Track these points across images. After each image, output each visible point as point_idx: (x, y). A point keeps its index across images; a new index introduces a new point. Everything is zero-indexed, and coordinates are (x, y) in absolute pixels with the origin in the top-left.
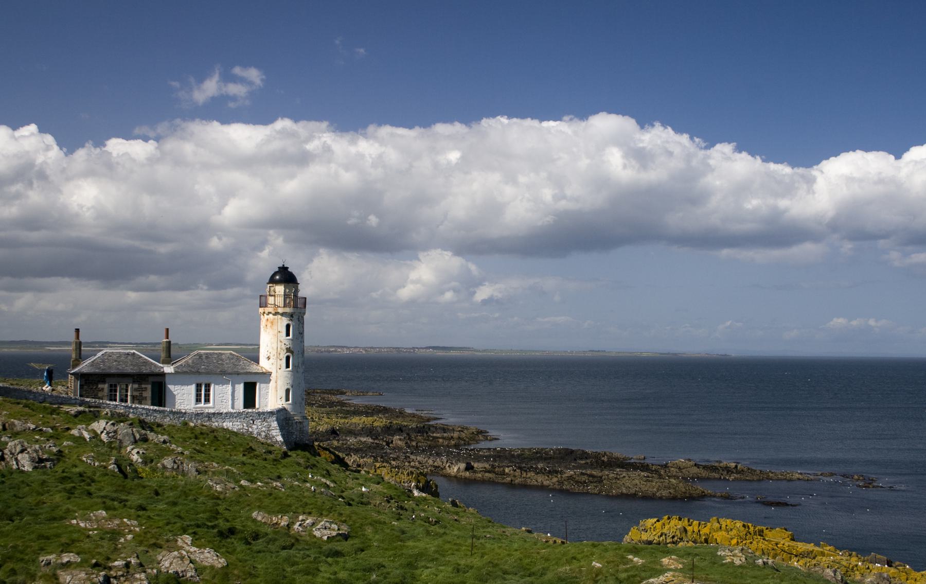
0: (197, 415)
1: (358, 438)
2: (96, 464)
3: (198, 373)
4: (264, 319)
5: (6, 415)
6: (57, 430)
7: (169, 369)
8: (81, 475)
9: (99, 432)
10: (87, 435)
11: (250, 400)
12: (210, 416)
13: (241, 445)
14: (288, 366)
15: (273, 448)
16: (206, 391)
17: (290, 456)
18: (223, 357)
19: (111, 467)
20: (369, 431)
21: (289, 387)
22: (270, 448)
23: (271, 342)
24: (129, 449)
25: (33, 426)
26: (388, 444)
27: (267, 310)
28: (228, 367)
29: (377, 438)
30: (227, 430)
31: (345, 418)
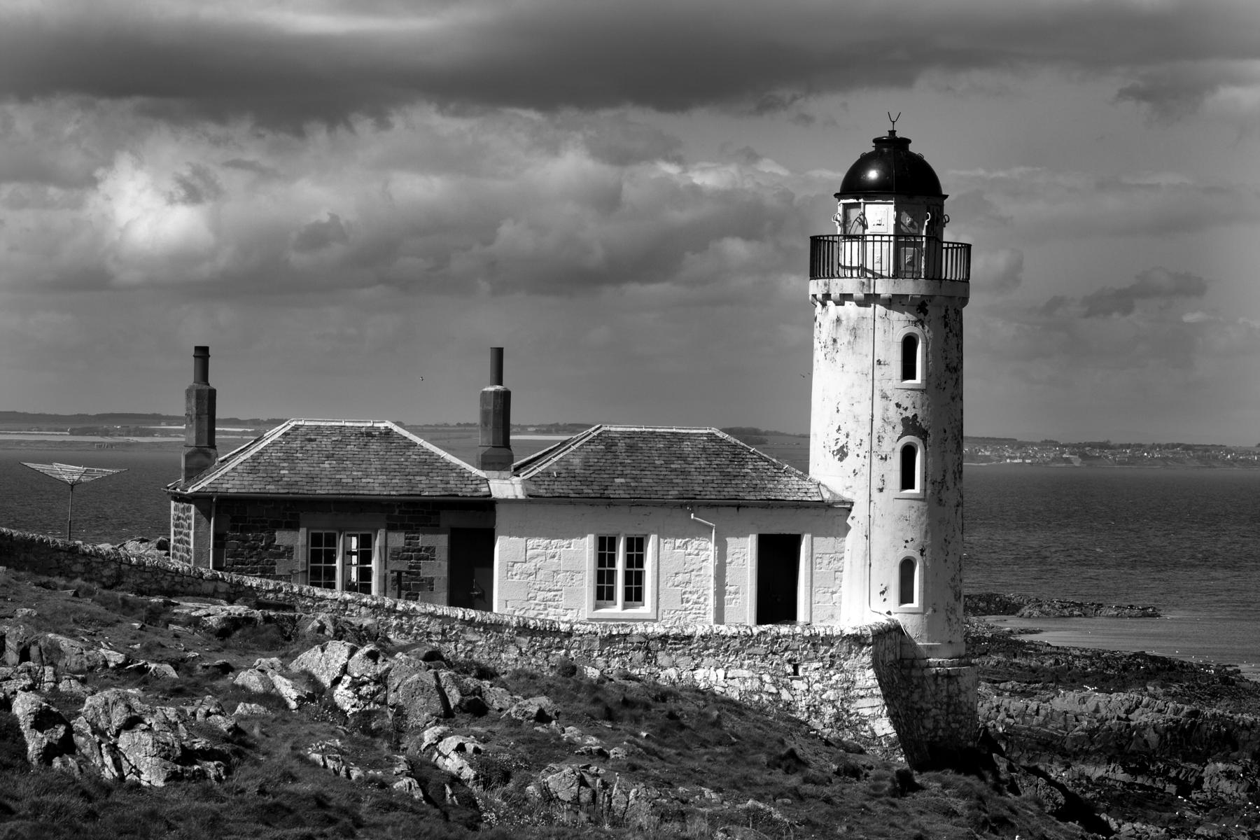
0: (609, 639)
1: (1078, 767)
2: (356, 773)
3: (604, 501)
4: (826, 316)
5: (27, 619)
6: (190, 671)
7: (505, 487)
8: (320, 801)
9: (326, 681)
10: (289, 691)
11: (776, 598)
12: (650, 646)
13: (759, 745)
14: (907, 482)
15: (862, 761)
16: (629, 562)
17: (919, 788)
18: (687, 447)
19: (402, 784)
20: (1118, 744)
21: (912, 552)
22: (853, 759)
23: (847, 393)
24: (428, 736)
25: (116, 658)
26: (1184, 789)
27: (838, 286)
28: (701, 481)
29: (1142, 770)
30: (706, 695)
31: (1024, 694)
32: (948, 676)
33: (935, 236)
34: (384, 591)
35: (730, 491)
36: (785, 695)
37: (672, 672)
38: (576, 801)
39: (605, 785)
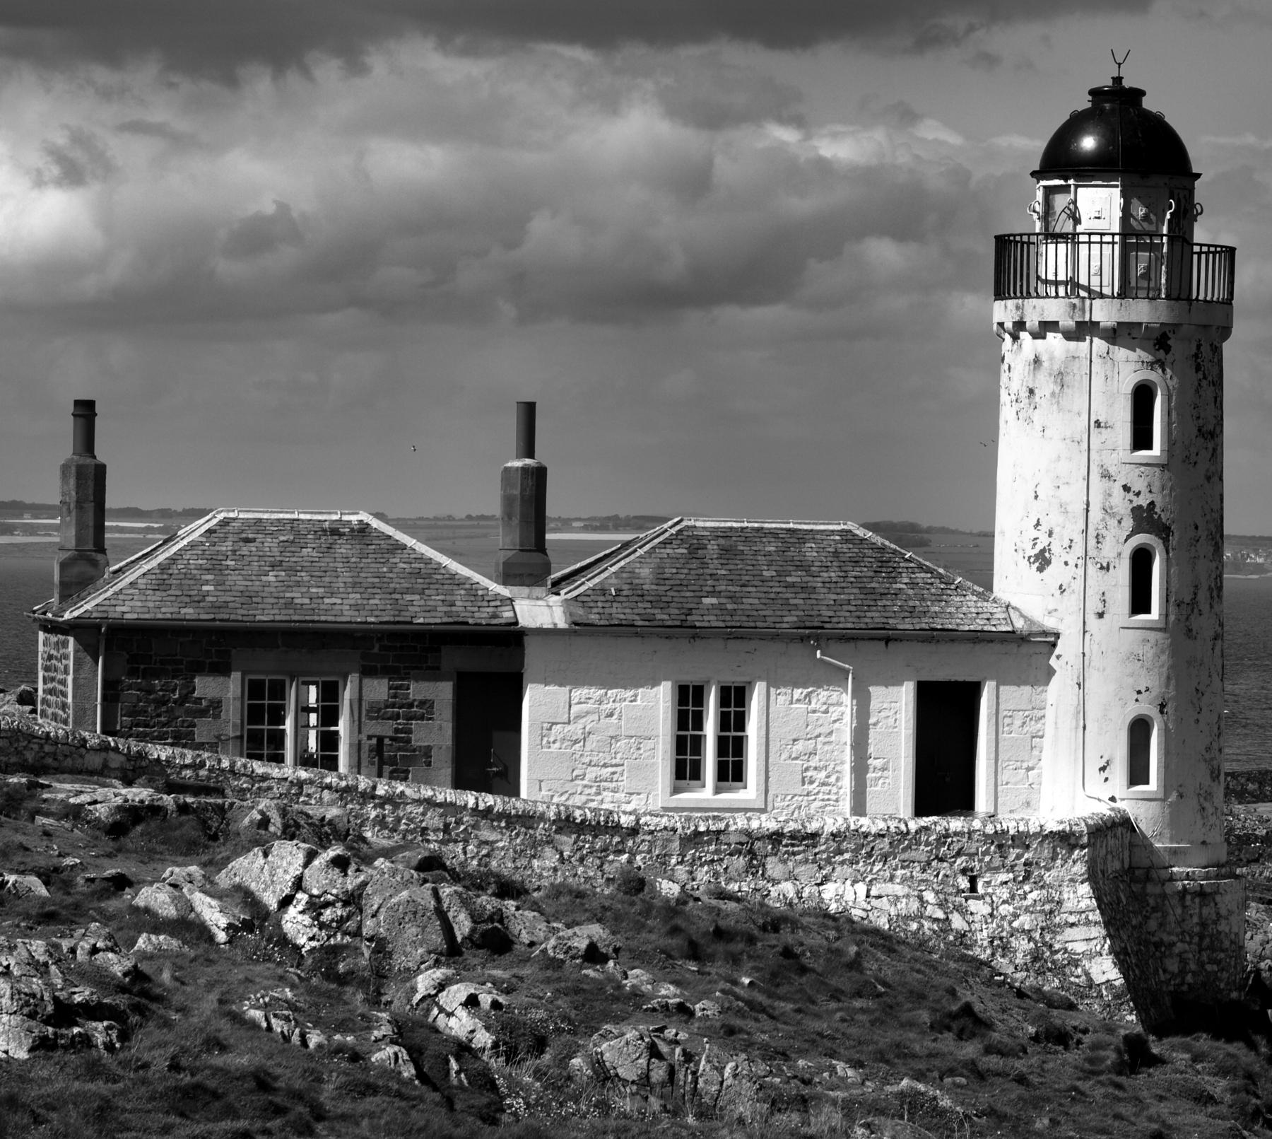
0: (695, 839)
2: (315, 1039)
3: (686, 631)
4: (1018, 356)
6: (67, 886)
9: (271, 902)
10: (214, 916)
11: (945, 776)
12: (755, 849)
13: (918, 997)
14: (1140, 602)
15: (1072, 1020)
16: (724, 722)
17: (1157, 1061)
21: (1147, 708)
22: (1058, 1017)
24: (424, 983)
27: (1036, 310)
30: (839, 922)
32: (1202, 894)
34: (357, 767)
36: (957, 922)
37: (788, 888)
38: (645, 1080)
39: (688, 1057)
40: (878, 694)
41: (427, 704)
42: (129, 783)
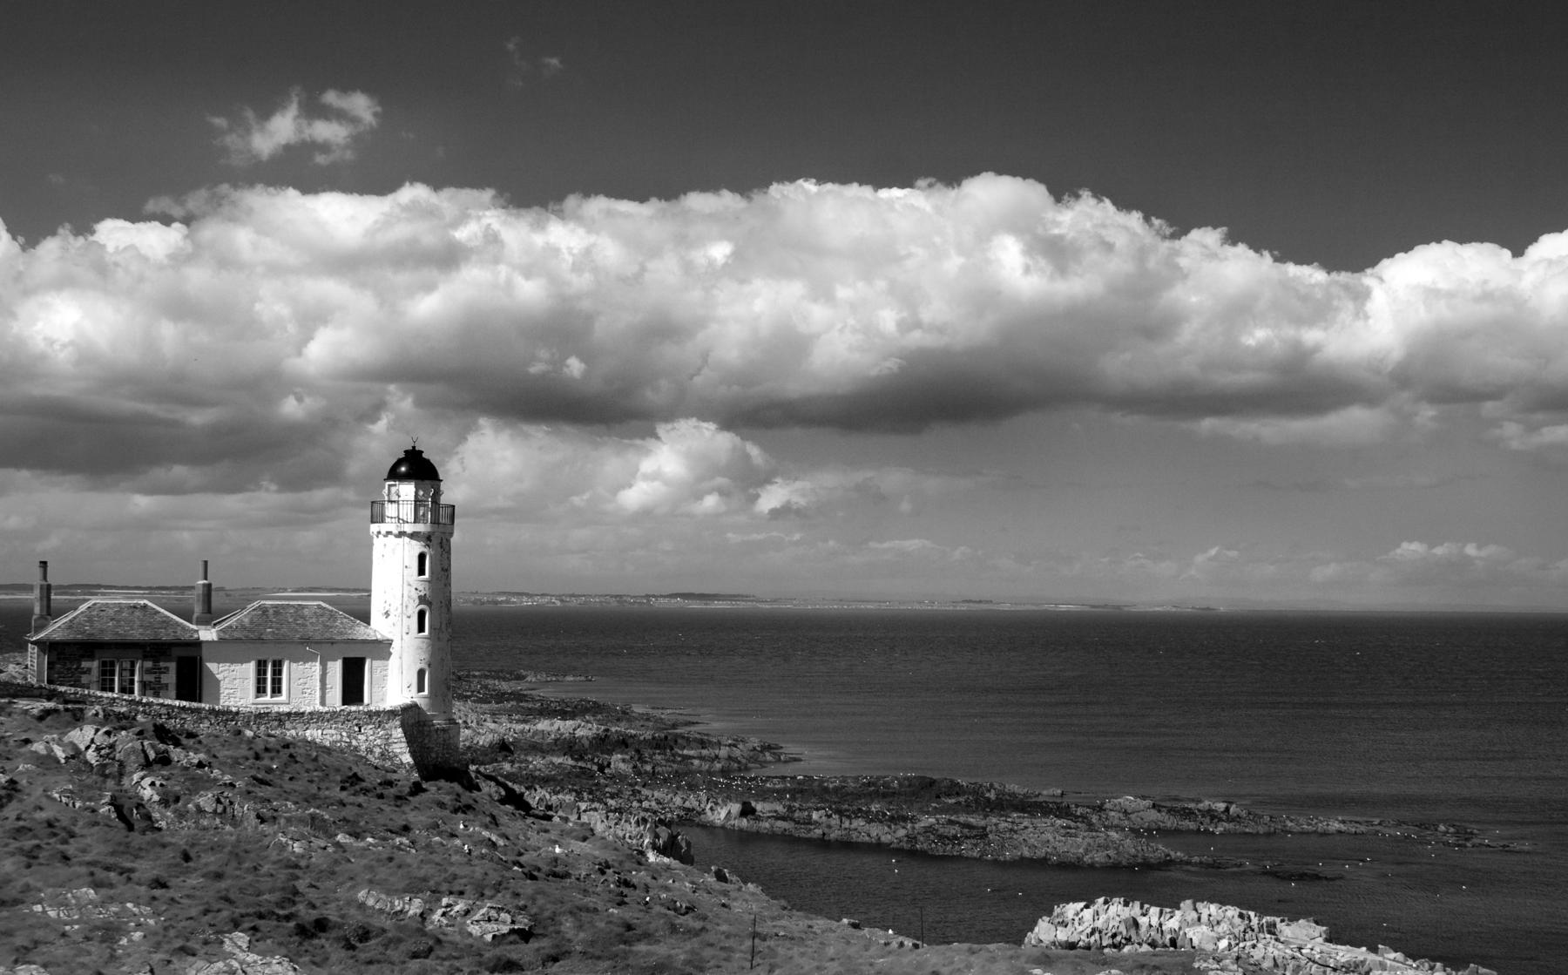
0: (260, 716)
1: (549, 758)
4: (378, 543)
9: (82, 747)
10: (60, 753)
11: (353, 690)
12: (282, 719)
13: (338, 770)
14: (421, 629)
15: (394, 777)
16: (274, 673)
17: (425, 790)
18: (306, 612)
20: (569, 746)
26: (601, 769)
27: (384, 528)
29: (581, 758)
30: (312, 744)
31: (525, 722)
32: (444, 730)
33: (436, 501)
34: (143, 693)
35: (328, 635)
36: (354, 743)
37: (293, 732)
38: (215, 811)
39: (231, 803)
40: (330, 664)
41: (167, 668)
42: (49, 700)
